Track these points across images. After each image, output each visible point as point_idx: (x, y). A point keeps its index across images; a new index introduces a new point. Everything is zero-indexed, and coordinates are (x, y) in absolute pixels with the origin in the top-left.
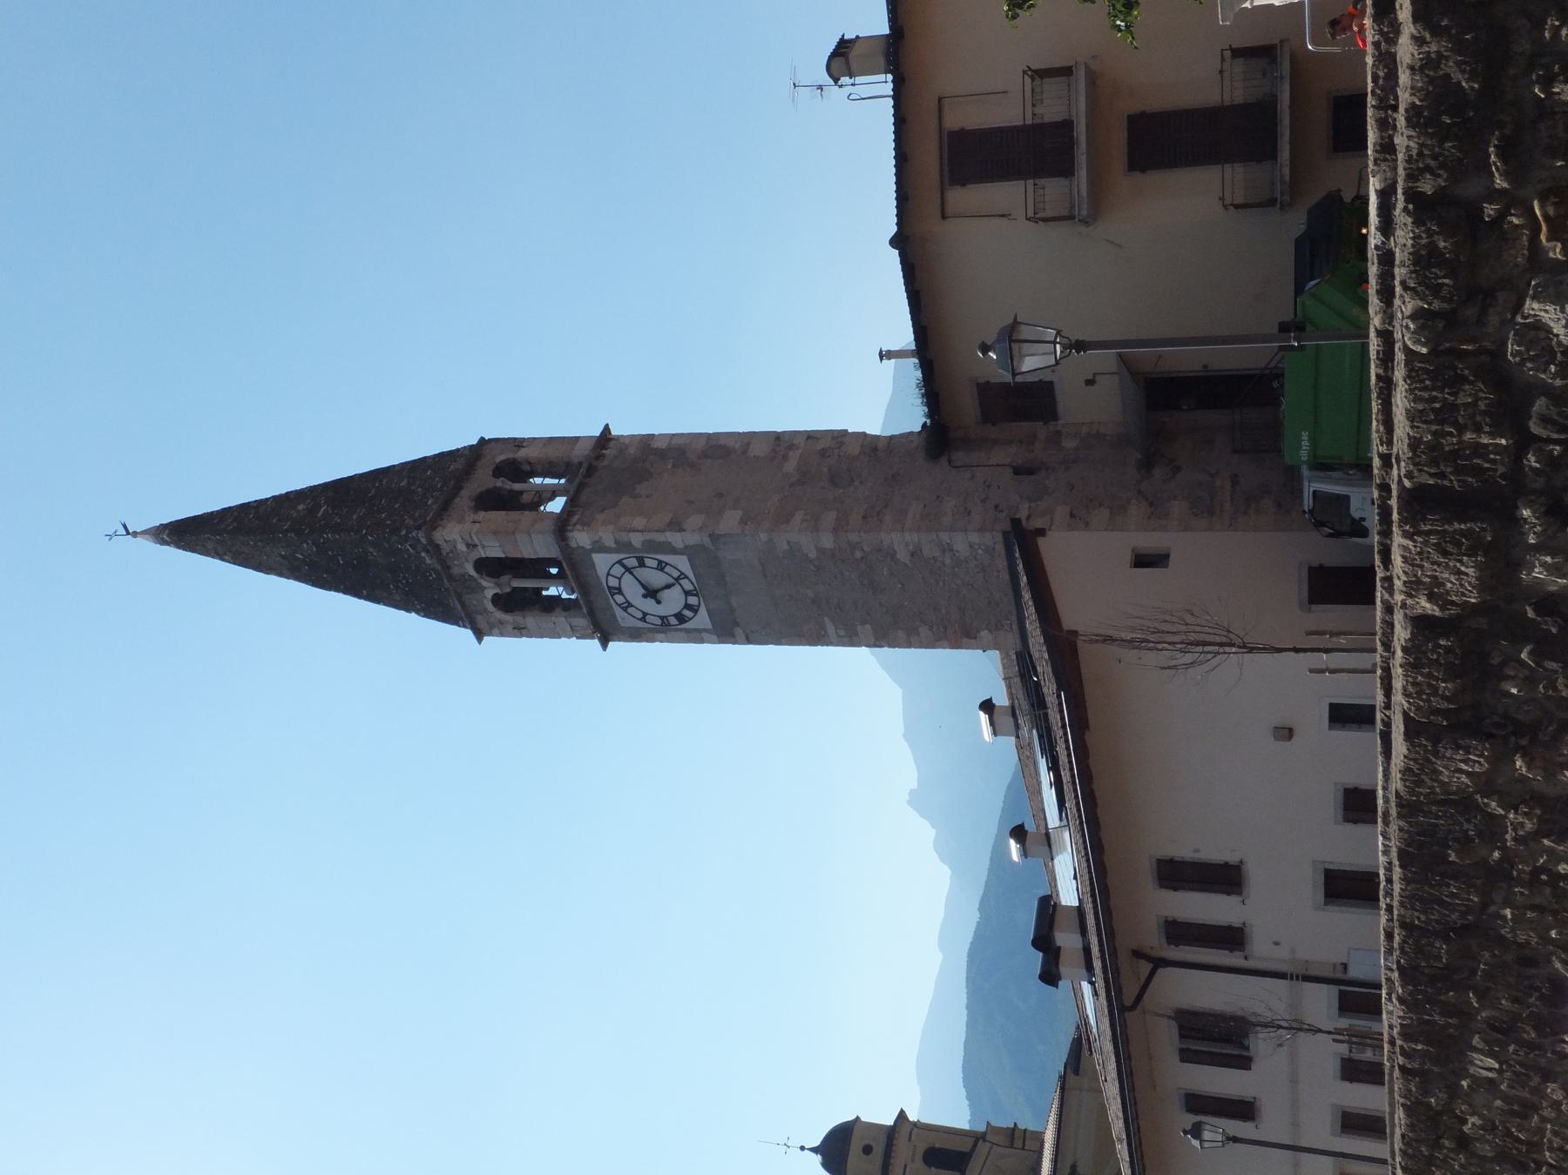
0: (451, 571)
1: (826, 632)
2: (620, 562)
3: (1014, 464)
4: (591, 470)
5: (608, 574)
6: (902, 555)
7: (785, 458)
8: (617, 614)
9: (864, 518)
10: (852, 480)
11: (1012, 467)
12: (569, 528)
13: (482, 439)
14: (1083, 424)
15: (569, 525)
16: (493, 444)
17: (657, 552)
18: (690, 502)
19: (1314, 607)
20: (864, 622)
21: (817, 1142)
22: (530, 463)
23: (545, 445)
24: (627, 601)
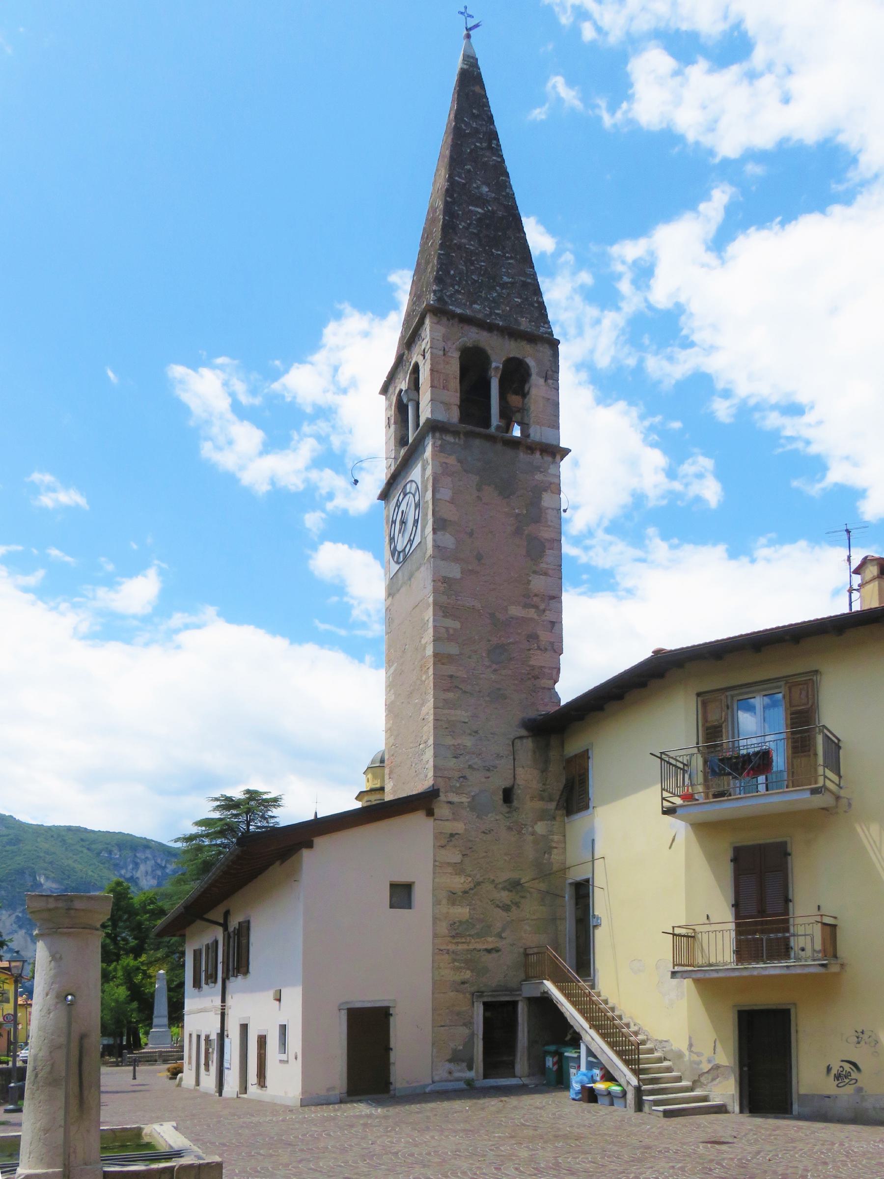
0: (551, 466)
3: (515, 787)
5: (412, 481)
7: (526, 606)
9: (451, 676)
11: (513, 786)
12: (437, 435)
13: (558, 342)
14: (564, 836)
19: (344, 1014)
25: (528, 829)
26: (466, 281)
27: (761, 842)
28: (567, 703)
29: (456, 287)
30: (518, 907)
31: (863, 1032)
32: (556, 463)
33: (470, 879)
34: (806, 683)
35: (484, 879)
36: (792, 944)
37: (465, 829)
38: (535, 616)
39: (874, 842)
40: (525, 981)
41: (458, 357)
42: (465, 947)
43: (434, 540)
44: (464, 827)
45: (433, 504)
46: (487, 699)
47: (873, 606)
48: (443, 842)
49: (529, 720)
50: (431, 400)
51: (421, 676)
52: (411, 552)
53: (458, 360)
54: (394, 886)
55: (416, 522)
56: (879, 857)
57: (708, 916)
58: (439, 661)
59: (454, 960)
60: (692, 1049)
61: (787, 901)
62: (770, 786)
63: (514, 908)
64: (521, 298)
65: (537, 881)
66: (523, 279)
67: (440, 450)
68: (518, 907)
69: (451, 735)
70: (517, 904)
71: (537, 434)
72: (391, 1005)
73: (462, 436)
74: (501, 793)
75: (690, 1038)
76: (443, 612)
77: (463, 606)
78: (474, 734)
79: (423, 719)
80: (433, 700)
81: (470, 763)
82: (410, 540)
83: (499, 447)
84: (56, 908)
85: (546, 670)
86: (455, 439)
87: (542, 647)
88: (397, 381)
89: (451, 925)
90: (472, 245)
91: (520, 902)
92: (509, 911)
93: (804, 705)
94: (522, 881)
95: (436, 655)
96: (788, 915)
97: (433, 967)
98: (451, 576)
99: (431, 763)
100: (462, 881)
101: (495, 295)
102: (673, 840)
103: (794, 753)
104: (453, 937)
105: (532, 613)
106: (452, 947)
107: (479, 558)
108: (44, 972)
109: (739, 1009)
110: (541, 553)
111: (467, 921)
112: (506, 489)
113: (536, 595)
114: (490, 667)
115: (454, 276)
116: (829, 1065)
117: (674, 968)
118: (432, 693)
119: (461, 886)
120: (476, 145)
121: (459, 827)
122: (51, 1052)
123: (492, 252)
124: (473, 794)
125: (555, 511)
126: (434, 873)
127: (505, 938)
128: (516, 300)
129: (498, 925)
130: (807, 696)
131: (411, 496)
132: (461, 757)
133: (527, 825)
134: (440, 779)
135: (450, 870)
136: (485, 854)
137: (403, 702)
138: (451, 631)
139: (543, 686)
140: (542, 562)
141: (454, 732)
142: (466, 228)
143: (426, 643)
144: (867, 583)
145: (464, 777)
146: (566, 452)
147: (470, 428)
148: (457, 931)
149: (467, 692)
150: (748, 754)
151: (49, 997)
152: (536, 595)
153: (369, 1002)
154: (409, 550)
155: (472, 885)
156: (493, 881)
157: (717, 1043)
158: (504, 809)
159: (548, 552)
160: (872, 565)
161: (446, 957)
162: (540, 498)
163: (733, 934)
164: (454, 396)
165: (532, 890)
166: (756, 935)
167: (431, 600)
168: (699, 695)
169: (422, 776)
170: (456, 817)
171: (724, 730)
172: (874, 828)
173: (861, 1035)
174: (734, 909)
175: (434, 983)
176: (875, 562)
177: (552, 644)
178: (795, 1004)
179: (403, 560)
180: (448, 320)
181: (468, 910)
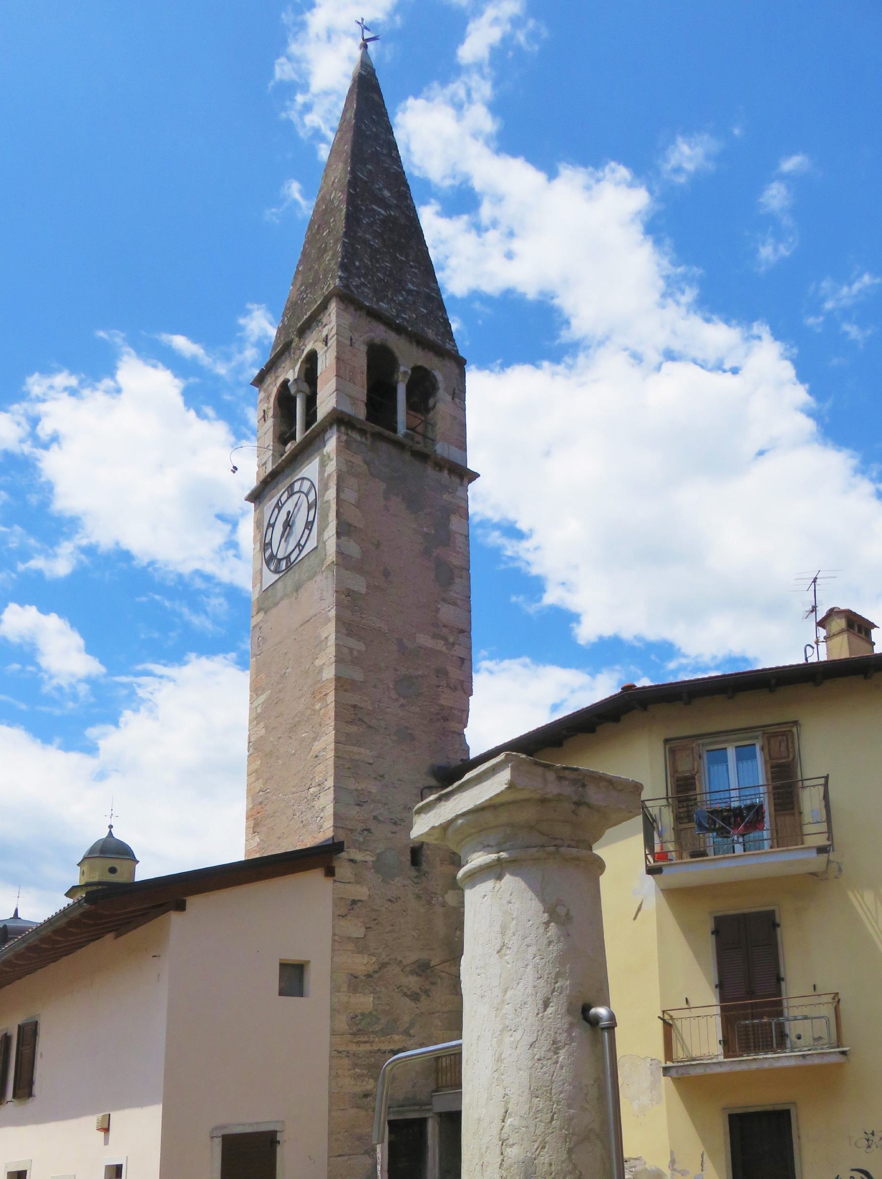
1: (262, 694)
2: (313, 485)
4: (423, 457)
5: (303, 479)
6: (317, 746)
7: (435, 636)
8: (273, 500)
9: (355, 706)
10: (404, 697)
12: (343, 429)
15: (346, 429)
16: (457, 371)
17: (320, 521)
18: (378, 545)
19: (218, 1142)
20: (266, 727)
21: (116, 835)
22: (435, 406)
23: (455, 418)
24: (283, 505)
25: (438, 898)
26: (372, 277)
27: (745, 911)
28: (496, 747)
29: (362, 280)
30: (428, 996)
31: (873, 1134)
32: (464, 486)
33: (374, 959)
34: (784, 734)
35: (390, 960)
36: (787, 1031)
37: (369, 895)
38: (444, 649)
39: (868, 909)
40: (436, 1091)
41: (365, 351)
42: (368, 1047)
43: (338, 546)
44: (368, 893)
45: (337, 504)
46: (394, 738)
47: (843, 657)
48: (343, 911)
49: (440, 768)
50: (336, 390)
51: (314, 705)
52: (299, 559)
53: (365, 354)
54: (285, 967)
55: (309, 525)
56: (876, 928)
57: (687, 1000)
58: (341, 686)
59: (356, 1065)
60: (674, 1167)
61: (779, 979)
62: (747, 845)
63: (423, 997)
64: (426, 309)
65: (448, 963)
66: (427, 291)
67: (344, 447)
68: (428, 996)
69: (354, 777)
70: (427, 992)
71: (442, 449)
72: (278, 1129)
73: (368, 436)
74: (409, 853)
75: (672, 1153)
76: (347, 629)
77: (368, 626)
78: (380, 778)
79: (316, 756)
80: (334, 732)
81: (374, 814)
82: (298, 544)
83: (407, 456)
84: (559, 797)
85: (456, 712)
86: (361, 438)
87: (452, 686)
88: (280, 370)
89: (352, 1018)
90: (376, 243)
91: (429, 990)
92: (419, 1001)
93: (785, 758)
94: (432, 963)
95: (338, 679)
96: (781, 996)
97: (330, 1075)
98: (357, 590)
99: (330, 810)
100: (365, 962)
101: (401, 298)
102: (639, 909)
103: (776, 811)
104: (354, 1034)
105: (440, 645)
106: (353, 1048)
107: (386, 574)
108: (532, 950)
109: (730, 1113)
110: (450, 581)
111: (370, 1013)
112: (413, 503)
113: (444, 626)
114: (397, 700)
115: (358, 268)
116: (838, 1176)
117: (666, 1063)
118: (333, 724)
119: (363, 968)
120: (376, 149)
121: (361, 892)
122: (570, 1151)
123: (396, 256)
124: (378, 851)
125: (463, 536)
126: (333, 950)
127: (414, 1036)
128: (422, 309)
129: (406, 1019)
130: (787, 747)
131: (303, 496)
132: (365, 804)
133: (437, 894)
134: (340, 831)
135: (351, 946)
136: (391, 928)
137: (280, 738)
138: (355, 653)
139: (453, 729)
140: (451, 591)
141: (357, 774)
142: (371, 225)
143: (324, 664)
144: (834, 635)
145: (368, 830)
146: (474, 476)
147: (378, 429)
148: (359, 1027)
149: (372, 728)
150: (739, 808)
151: (550, 1010)
152: (444, 626)
153: (251, 1125)
154: (296, 558)
155: (376, 967)
156: (401, 961)
157: (704, 1158)
158: (413, 873)
159: (457, 580)
160: (839, 618)
161: (346, 1061)
162: (448, 520)
163: (719, 1020)
164: (361, 392)
165: (443, 974)
166: (762, 1018)
167: (333, 613)
168: (666, 741)
169: (313, 827)
170: (359, 880)
171: (697, 783)
172: (869, 897)
173: (871, 1138)
174: (718, 990)
175: (331, 1095)
176: (843, 615)
177: (462, 682)
178: (794, 1103)
179: (286, 569)
180: (356, 310)
181: (372, 999)
